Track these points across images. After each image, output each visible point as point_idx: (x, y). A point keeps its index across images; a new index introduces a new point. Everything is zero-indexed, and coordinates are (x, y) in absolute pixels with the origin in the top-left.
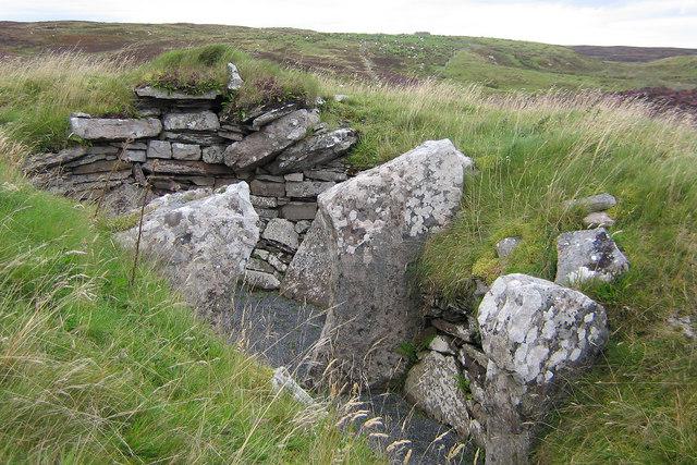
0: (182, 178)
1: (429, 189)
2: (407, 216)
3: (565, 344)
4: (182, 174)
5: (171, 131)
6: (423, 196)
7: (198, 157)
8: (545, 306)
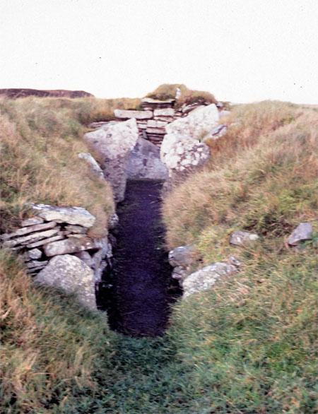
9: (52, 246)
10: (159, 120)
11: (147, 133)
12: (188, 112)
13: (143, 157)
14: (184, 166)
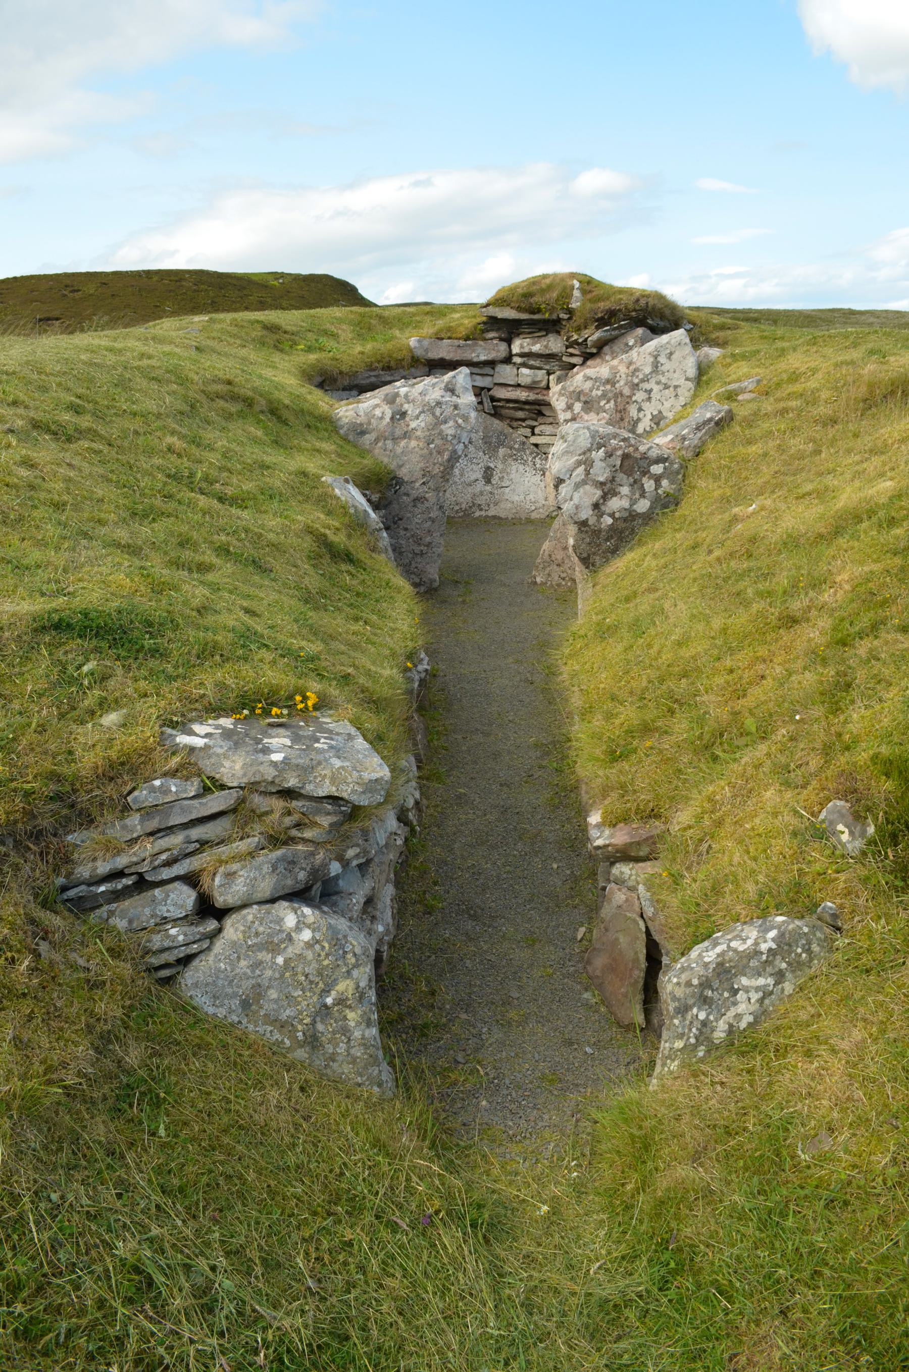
0: (527, 407)
1: (658, 383)
2: (633, 412)
3: (625, 490)
4: (526, 402)
5: (516, 355)
6: (651, 391)
7: (544, 384)
8: (595, 446)
9: (230, 875)
10: (524, 365)
11: (493, 399)
12: (601, 345)
13: (484, 459)
14: (612, 515)
